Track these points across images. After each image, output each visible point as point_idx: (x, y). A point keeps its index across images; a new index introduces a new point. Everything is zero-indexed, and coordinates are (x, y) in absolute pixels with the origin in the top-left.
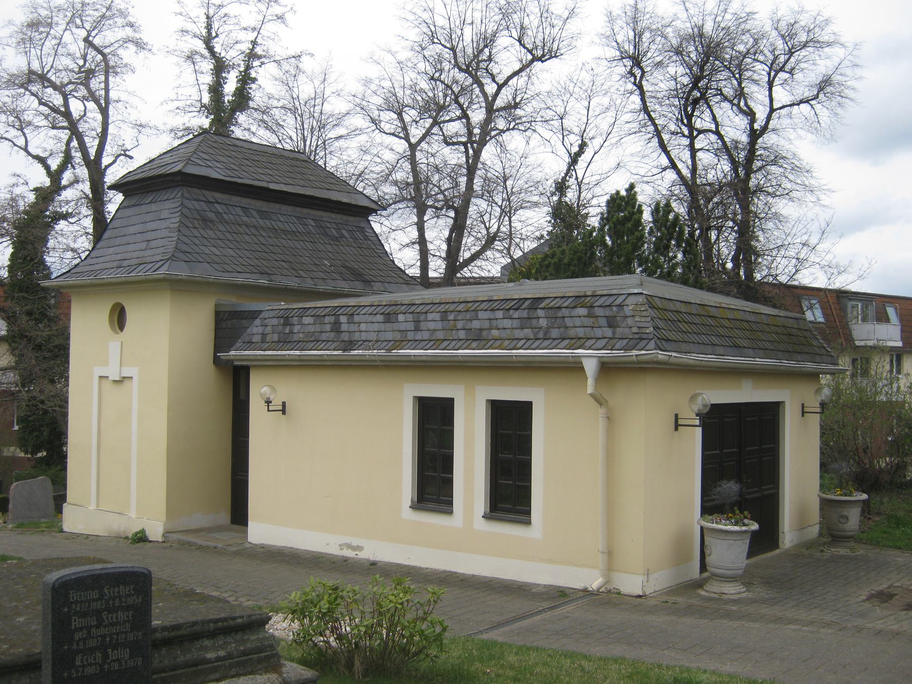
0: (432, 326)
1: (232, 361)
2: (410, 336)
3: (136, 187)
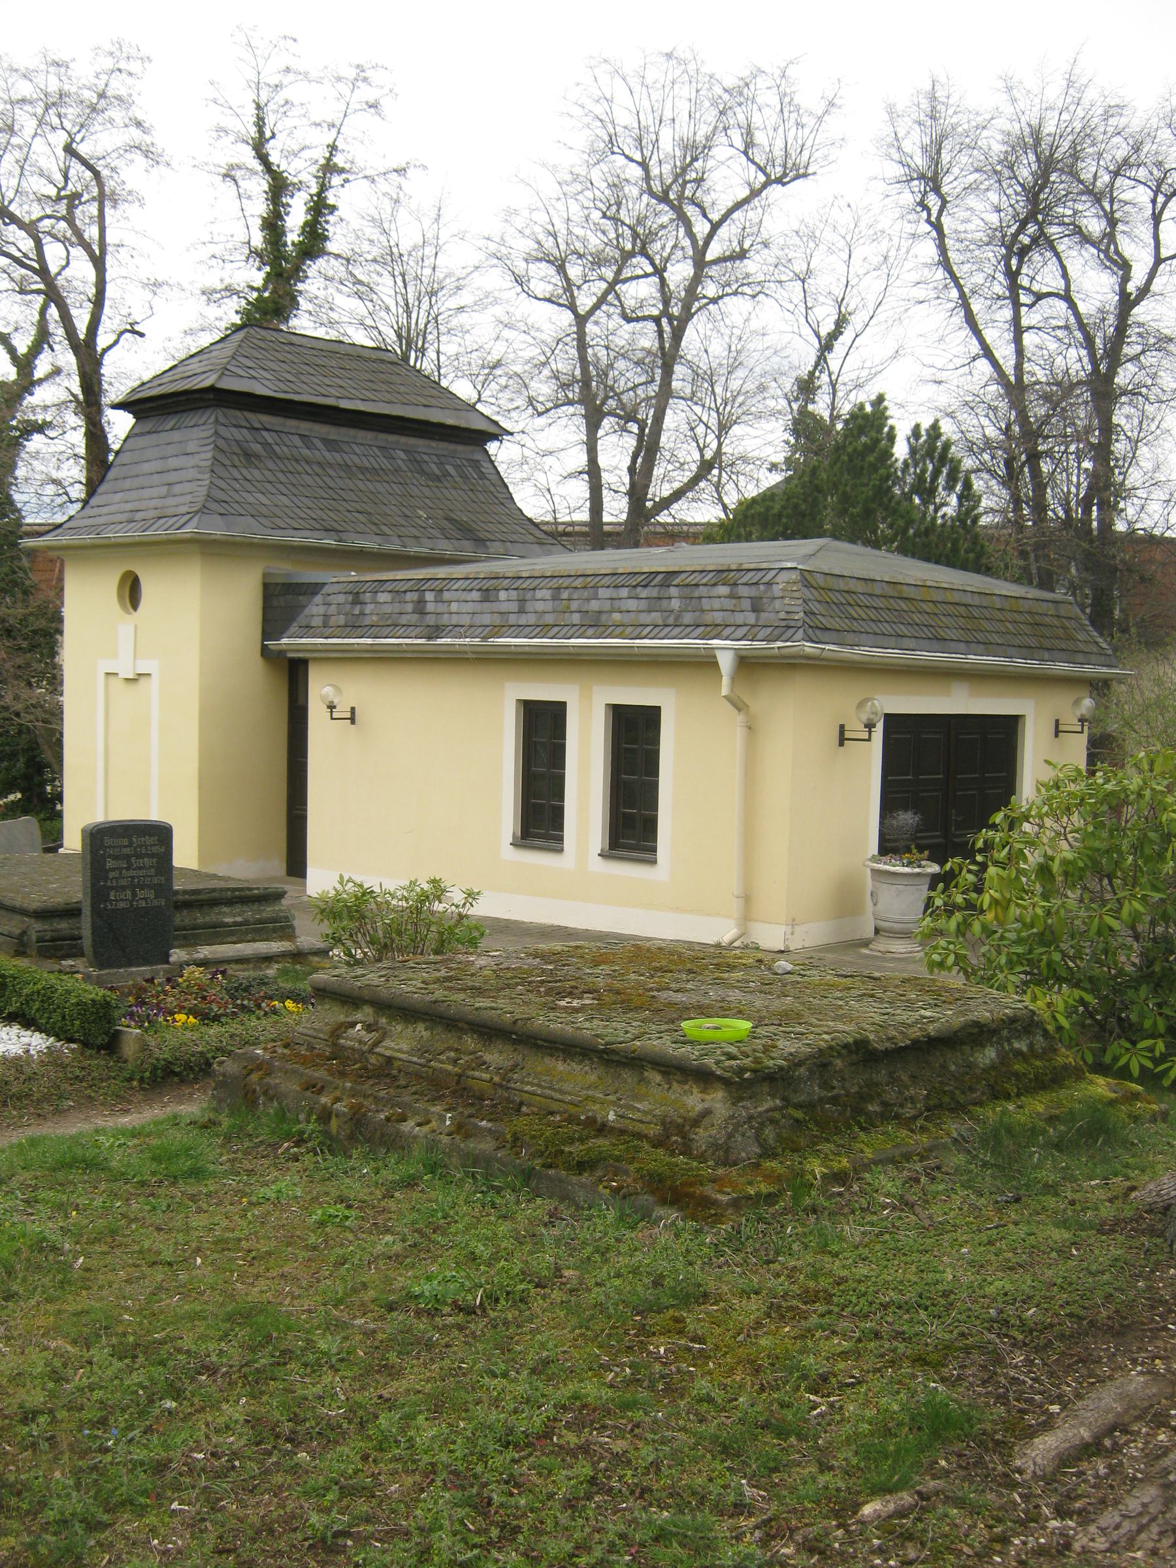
0: (540, 606)
2: (513, 619)
3: (153, 406)
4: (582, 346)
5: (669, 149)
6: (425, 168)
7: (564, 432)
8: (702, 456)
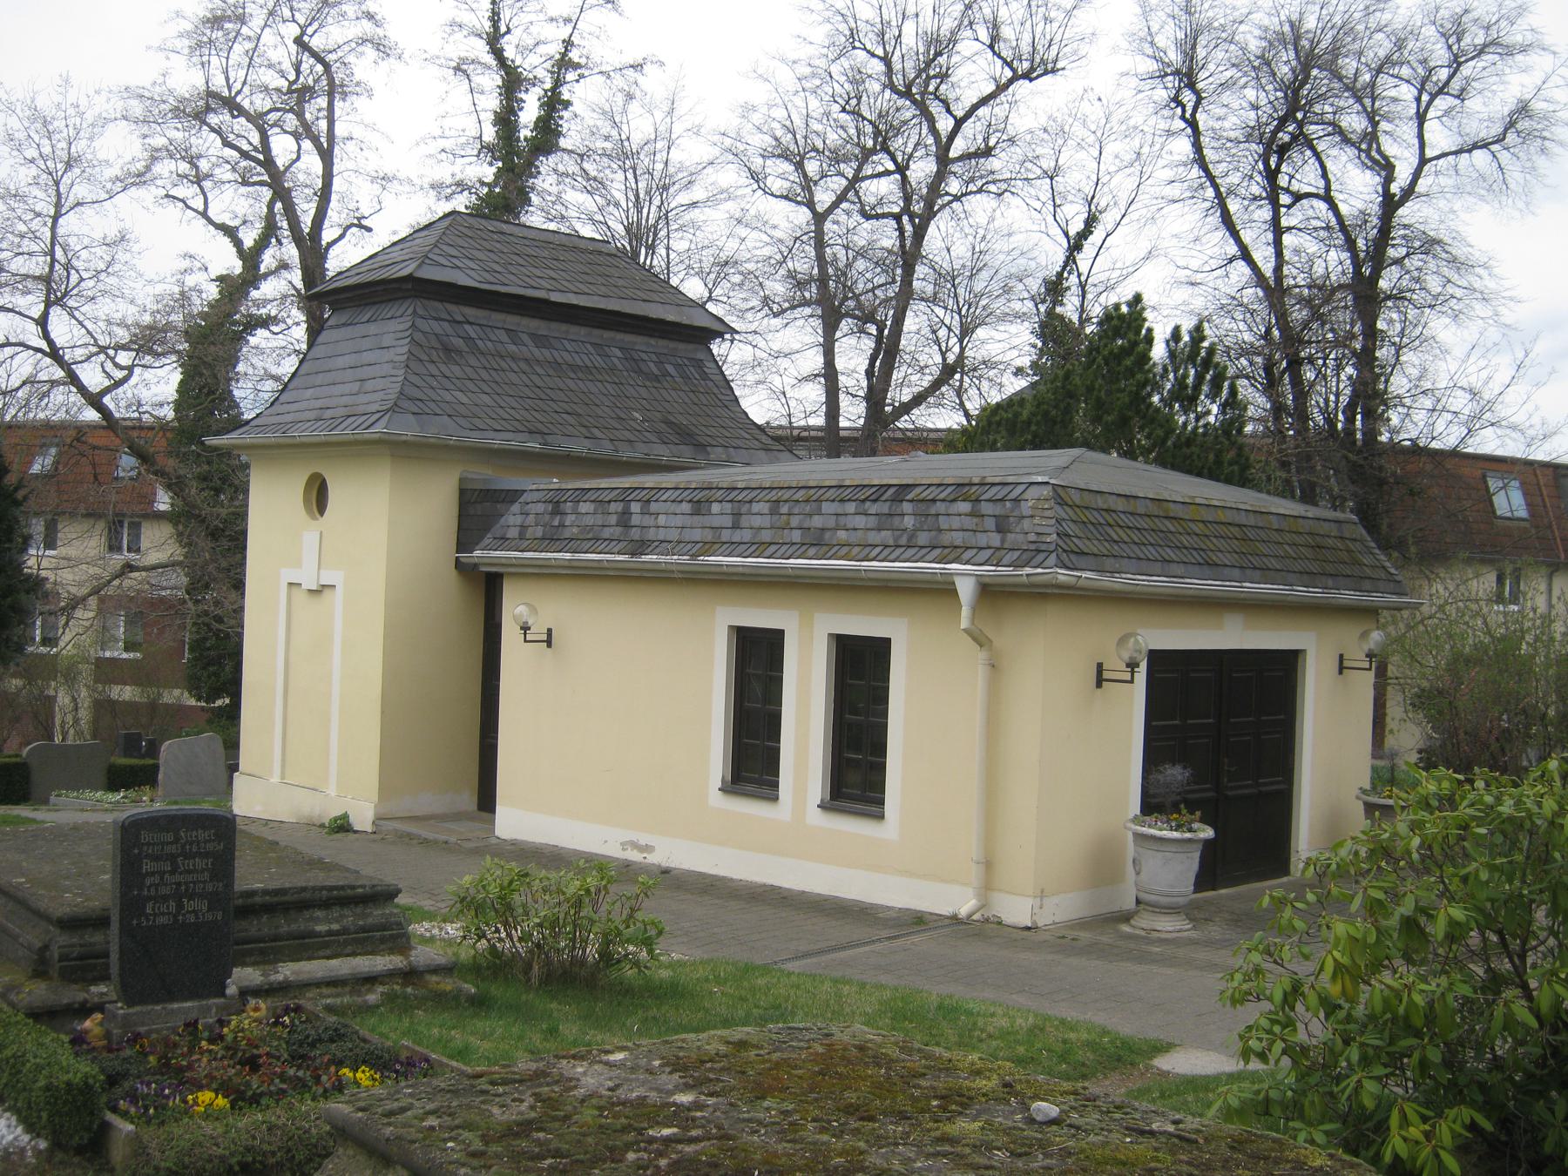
0: (757, 521)
1: (476, 565)
2: (726, 535)
4: (820, 244)
5: (912, 43)
6: (662, 64)
7: (800, 335)
8: (944, 359)
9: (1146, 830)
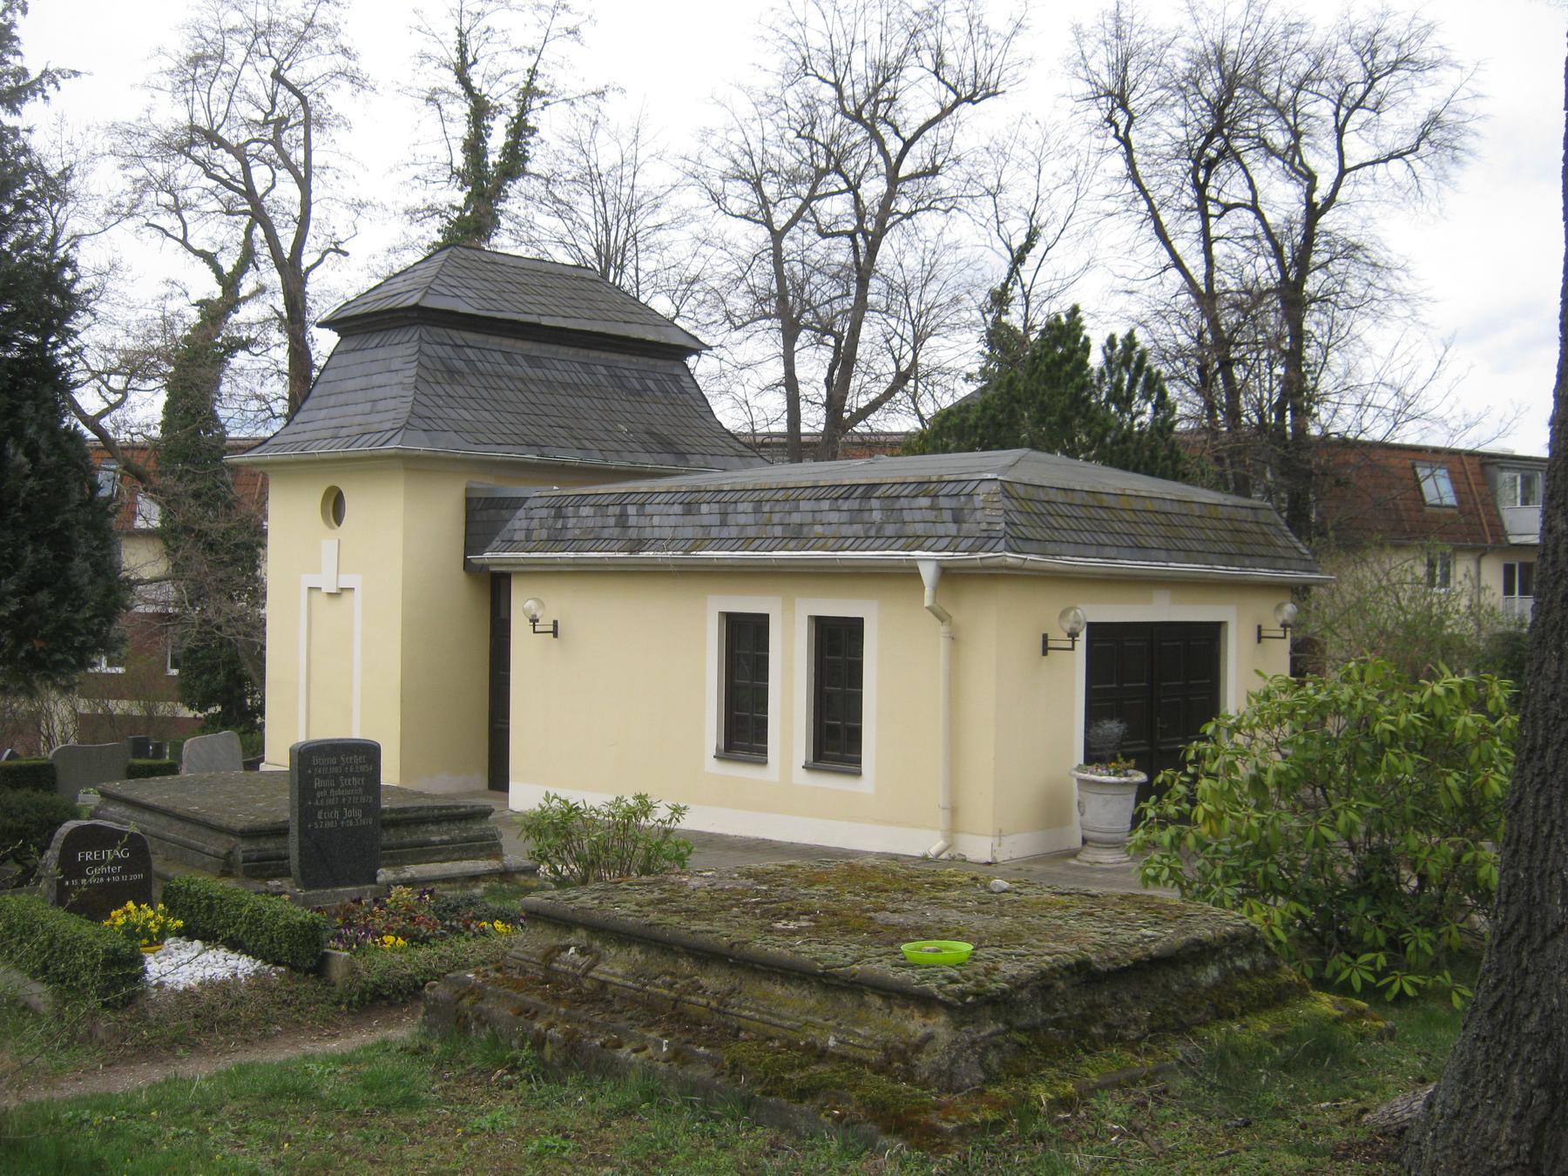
0: (742, 519)
1: (487, 566)
2: (714, 532)
3: (355, 324)
4: (778, 260)
6: (623, 91)
7: (760, 348)
8: (898, 367)
9: (1088, 776)
